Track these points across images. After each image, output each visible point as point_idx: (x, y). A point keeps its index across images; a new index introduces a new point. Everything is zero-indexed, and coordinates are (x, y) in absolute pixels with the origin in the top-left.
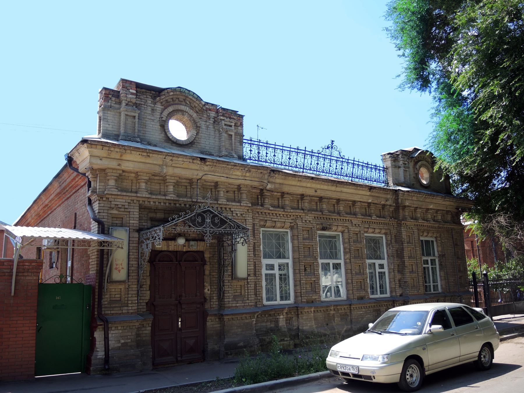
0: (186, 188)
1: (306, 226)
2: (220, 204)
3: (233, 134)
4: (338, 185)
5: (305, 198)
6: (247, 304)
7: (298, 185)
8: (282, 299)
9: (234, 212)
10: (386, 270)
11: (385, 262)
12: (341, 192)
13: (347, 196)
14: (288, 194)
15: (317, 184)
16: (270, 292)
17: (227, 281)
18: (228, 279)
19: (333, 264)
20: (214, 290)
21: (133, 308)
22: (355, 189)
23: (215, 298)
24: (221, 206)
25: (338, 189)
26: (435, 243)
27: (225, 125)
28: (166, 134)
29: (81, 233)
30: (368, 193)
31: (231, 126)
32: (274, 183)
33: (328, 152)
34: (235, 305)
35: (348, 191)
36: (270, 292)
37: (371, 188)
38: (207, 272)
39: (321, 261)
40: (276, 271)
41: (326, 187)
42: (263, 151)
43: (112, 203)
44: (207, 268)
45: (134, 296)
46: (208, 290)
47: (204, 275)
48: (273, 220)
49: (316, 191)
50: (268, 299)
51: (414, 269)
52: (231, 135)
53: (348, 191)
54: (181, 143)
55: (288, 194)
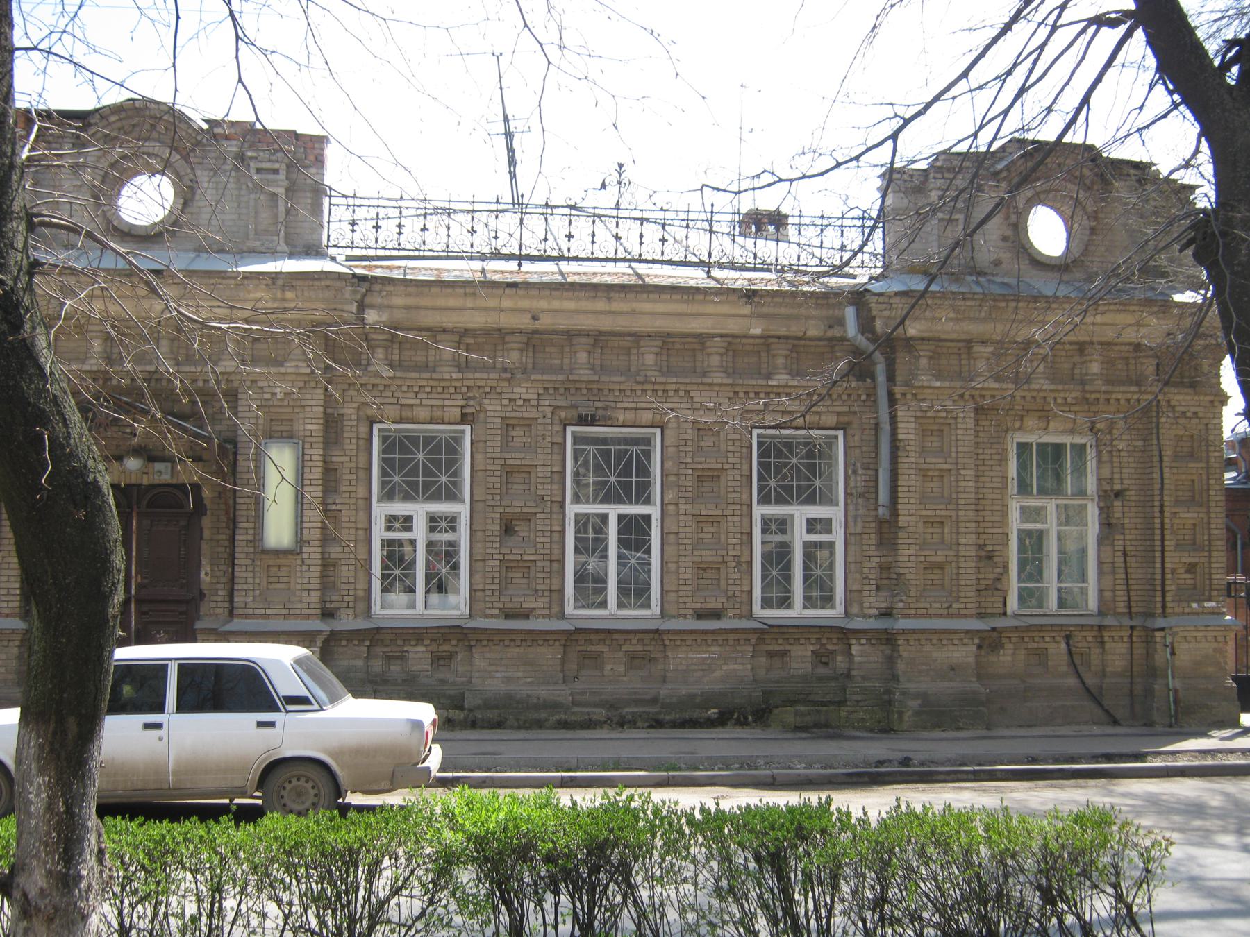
0: (1127, 364)
1: (518, 415)
2: (575, 381)
3: (281, 191)
4: (612, 294)
5: (708, 344)
6: (298, 612)
7: (469, 305)
8: (809, 601)
9: (1177, 409)
10: (837, 536)
11: (835, 513)
12: (633, 313)
13: (658, 323)
14: (444, 331)
15: (655, 301)
16: (590, 585)
17: (242, 556)
18: (246, 550)
19: (576, 515)
20: (218, 574)
21: (11, 605)
22: (687, 302)
23: (220, 592)
24: (1041, 394)
25: (617, 306)
26: (1090, 454)
27: (259, 171)
28: (1029, 255)
29: (1010, 463)
30: (746, 310)
31: (276, 171)
32: (390, 307)
33: (605, 200)
34: (262, 611)
35: (660, 308)
36: (590, 585)
37: (750, 295)
38: (207, 534)
39: (759, 511)
40: (420, 533)
41: (570, 305)
42: (629, 231)
43: (266, 390)
44: (206, 522)
45: (12, 579)
46: (207, 574)
47: (202, 538)
48: (403, 402)
49: (534, 318)
50: (767, 603)
51: (947, 537)
52: (274, 195)
53: (660, 308)
54: (143, 233)
55: (444, 331)
